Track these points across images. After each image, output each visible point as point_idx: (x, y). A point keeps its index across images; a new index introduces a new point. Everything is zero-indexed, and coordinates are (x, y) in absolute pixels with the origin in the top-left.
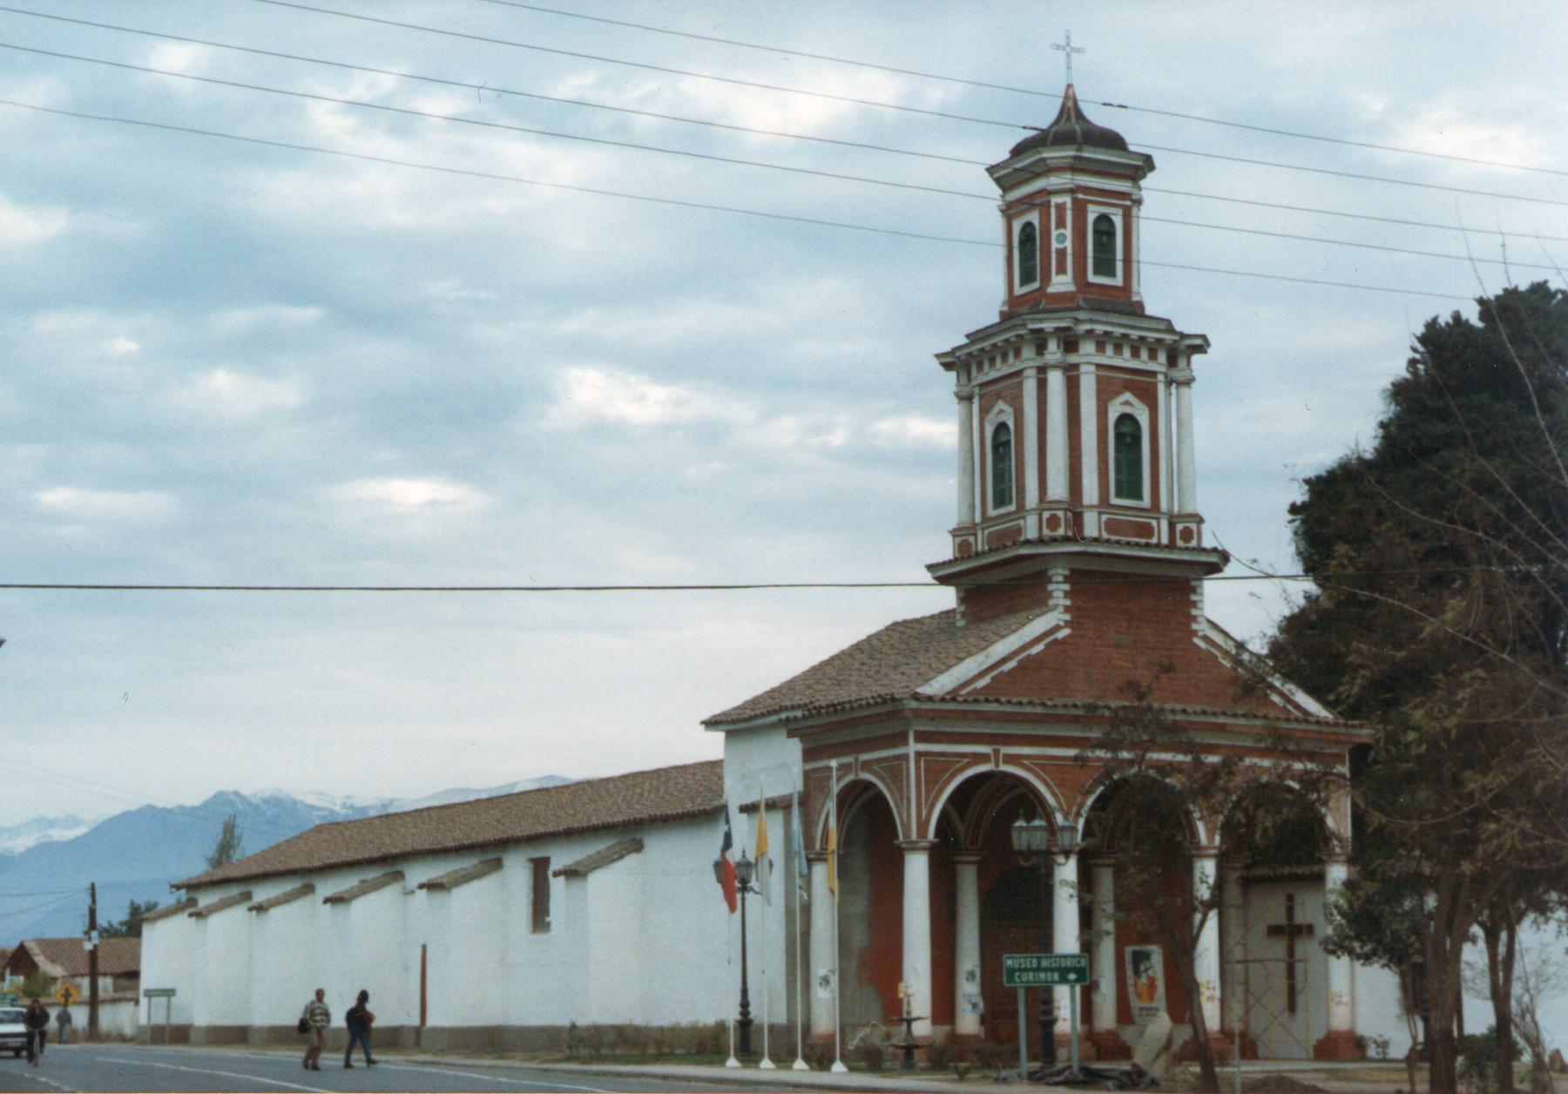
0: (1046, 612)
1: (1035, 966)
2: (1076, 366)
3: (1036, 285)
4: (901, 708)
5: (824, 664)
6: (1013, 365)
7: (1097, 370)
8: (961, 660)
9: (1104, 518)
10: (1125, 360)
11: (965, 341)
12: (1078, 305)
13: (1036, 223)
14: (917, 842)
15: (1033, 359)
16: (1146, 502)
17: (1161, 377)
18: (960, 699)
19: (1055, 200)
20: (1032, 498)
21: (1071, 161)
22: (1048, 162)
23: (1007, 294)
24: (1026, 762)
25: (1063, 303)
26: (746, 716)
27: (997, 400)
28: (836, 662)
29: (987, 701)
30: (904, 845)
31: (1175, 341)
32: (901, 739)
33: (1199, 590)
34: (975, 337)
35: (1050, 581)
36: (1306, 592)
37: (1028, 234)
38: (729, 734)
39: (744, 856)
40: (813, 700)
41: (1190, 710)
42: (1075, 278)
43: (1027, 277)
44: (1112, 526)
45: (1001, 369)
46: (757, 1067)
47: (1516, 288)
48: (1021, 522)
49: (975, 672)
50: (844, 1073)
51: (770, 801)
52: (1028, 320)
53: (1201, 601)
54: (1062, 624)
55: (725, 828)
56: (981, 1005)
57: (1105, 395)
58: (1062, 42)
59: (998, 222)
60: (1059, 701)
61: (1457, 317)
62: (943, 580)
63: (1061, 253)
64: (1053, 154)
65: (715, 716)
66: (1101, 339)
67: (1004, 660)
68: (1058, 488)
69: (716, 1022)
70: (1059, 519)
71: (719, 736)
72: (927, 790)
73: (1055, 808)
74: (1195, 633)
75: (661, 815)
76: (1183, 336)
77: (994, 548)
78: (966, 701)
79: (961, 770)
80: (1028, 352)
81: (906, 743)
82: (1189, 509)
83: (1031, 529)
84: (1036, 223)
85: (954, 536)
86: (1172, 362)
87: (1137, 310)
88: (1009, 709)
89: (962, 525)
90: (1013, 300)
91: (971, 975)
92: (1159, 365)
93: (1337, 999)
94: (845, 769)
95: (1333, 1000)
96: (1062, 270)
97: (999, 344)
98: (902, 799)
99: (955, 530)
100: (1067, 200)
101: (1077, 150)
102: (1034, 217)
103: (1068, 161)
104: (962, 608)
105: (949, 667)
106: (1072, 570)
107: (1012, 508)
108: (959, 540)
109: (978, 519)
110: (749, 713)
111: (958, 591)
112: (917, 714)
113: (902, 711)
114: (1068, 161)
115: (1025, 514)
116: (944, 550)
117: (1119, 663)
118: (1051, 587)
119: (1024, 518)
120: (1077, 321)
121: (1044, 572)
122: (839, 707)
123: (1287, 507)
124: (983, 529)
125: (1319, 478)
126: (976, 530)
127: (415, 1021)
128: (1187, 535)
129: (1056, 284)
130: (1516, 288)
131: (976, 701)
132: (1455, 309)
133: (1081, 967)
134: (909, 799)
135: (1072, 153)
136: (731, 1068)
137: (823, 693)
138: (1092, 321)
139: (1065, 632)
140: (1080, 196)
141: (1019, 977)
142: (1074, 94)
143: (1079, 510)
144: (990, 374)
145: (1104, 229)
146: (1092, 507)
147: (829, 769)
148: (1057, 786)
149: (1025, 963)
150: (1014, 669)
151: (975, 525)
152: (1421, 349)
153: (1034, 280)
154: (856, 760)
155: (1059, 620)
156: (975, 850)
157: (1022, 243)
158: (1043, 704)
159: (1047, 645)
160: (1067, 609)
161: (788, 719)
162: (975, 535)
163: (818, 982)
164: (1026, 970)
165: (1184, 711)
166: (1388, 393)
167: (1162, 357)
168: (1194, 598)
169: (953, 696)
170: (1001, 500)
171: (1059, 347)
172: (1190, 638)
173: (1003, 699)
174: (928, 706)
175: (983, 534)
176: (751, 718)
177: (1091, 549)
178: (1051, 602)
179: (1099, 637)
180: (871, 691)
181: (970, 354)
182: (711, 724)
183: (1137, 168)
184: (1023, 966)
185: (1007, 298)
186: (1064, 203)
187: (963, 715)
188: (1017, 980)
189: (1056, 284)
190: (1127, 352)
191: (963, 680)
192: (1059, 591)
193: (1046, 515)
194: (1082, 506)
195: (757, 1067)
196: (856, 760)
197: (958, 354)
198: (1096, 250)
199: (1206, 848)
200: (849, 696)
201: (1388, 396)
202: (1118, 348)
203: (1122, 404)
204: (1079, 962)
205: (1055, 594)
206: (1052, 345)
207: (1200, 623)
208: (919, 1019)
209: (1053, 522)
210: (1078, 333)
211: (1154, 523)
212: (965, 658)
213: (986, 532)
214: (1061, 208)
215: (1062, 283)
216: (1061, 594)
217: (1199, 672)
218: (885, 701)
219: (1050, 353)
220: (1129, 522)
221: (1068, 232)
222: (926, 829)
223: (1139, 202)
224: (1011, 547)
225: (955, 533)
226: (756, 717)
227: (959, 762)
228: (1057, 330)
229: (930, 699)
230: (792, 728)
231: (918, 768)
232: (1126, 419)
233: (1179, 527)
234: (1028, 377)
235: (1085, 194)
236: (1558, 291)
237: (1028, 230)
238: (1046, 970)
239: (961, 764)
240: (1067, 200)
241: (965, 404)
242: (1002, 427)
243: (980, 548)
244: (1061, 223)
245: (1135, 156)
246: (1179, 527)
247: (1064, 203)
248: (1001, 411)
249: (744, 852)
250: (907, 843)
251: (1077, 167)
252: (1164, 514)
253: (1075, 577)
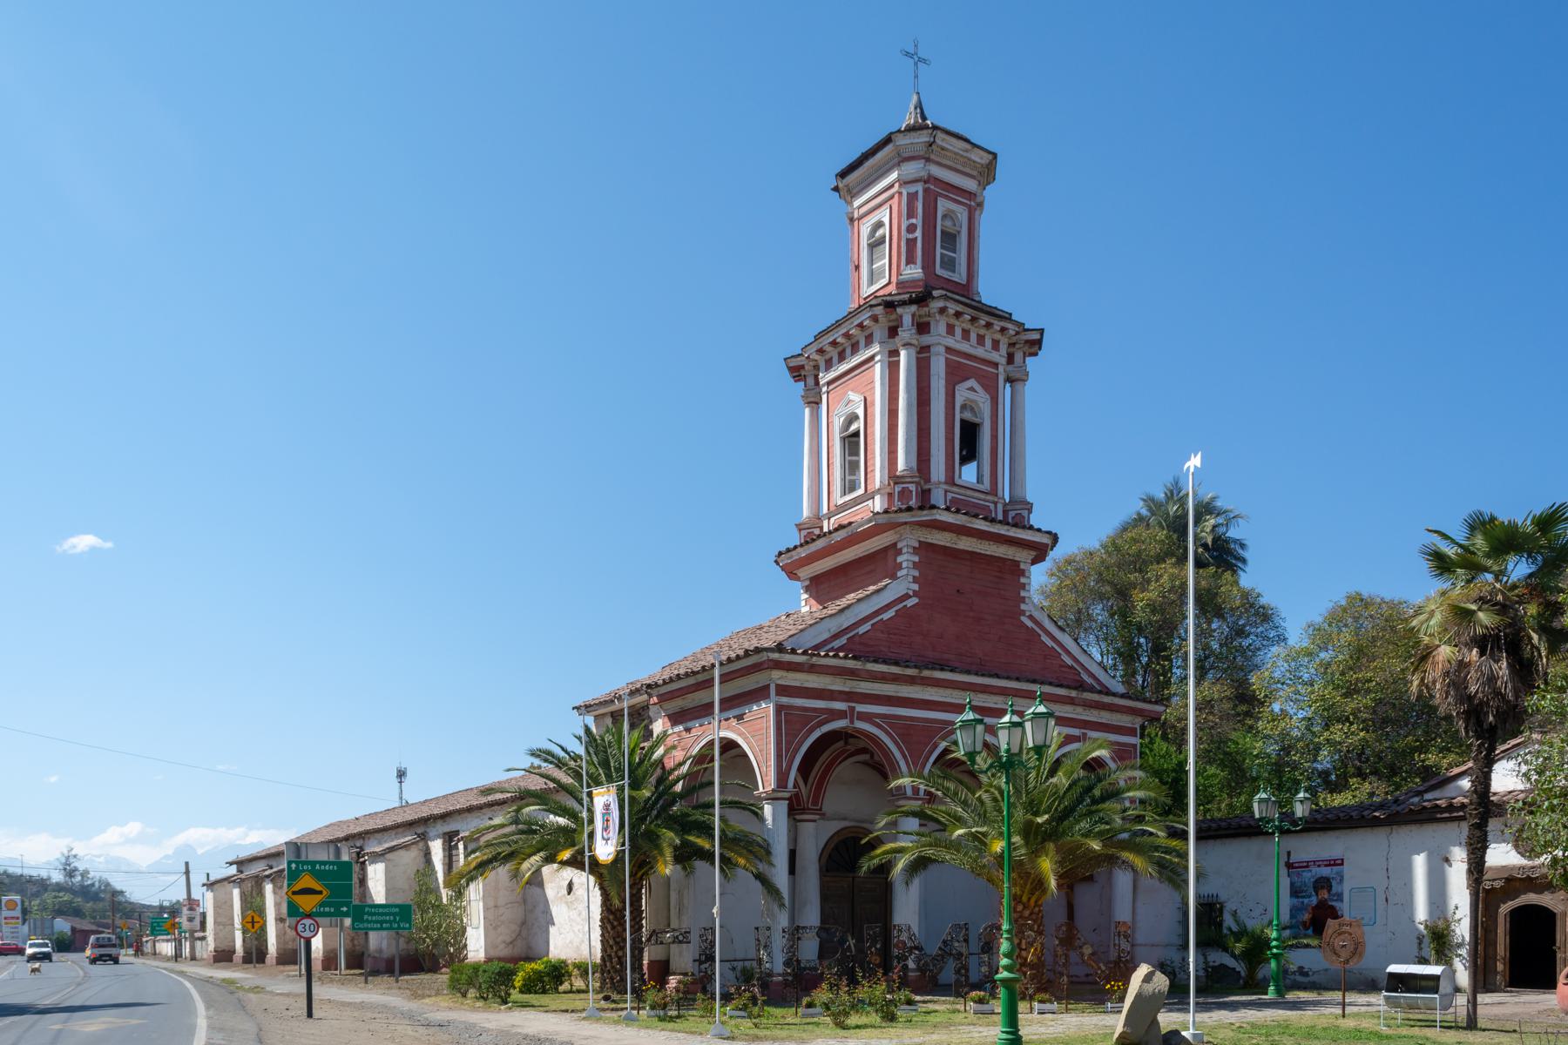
7: (946, 352)
9: (950, 496)
24: (877, 720)
53: (1029, 584)
54: (911, 594)
57: (956, 374)
73: (807, 660)
74: (1023, 613)
96: (607, 807)
127: (1347, 993)
139: (914, 601)
147: (590, 857)
160: (915, 580)
203: (968, 389)
209: (904, 494)
211: (992, 506)
223: (980, 205)
247: (917, 192)
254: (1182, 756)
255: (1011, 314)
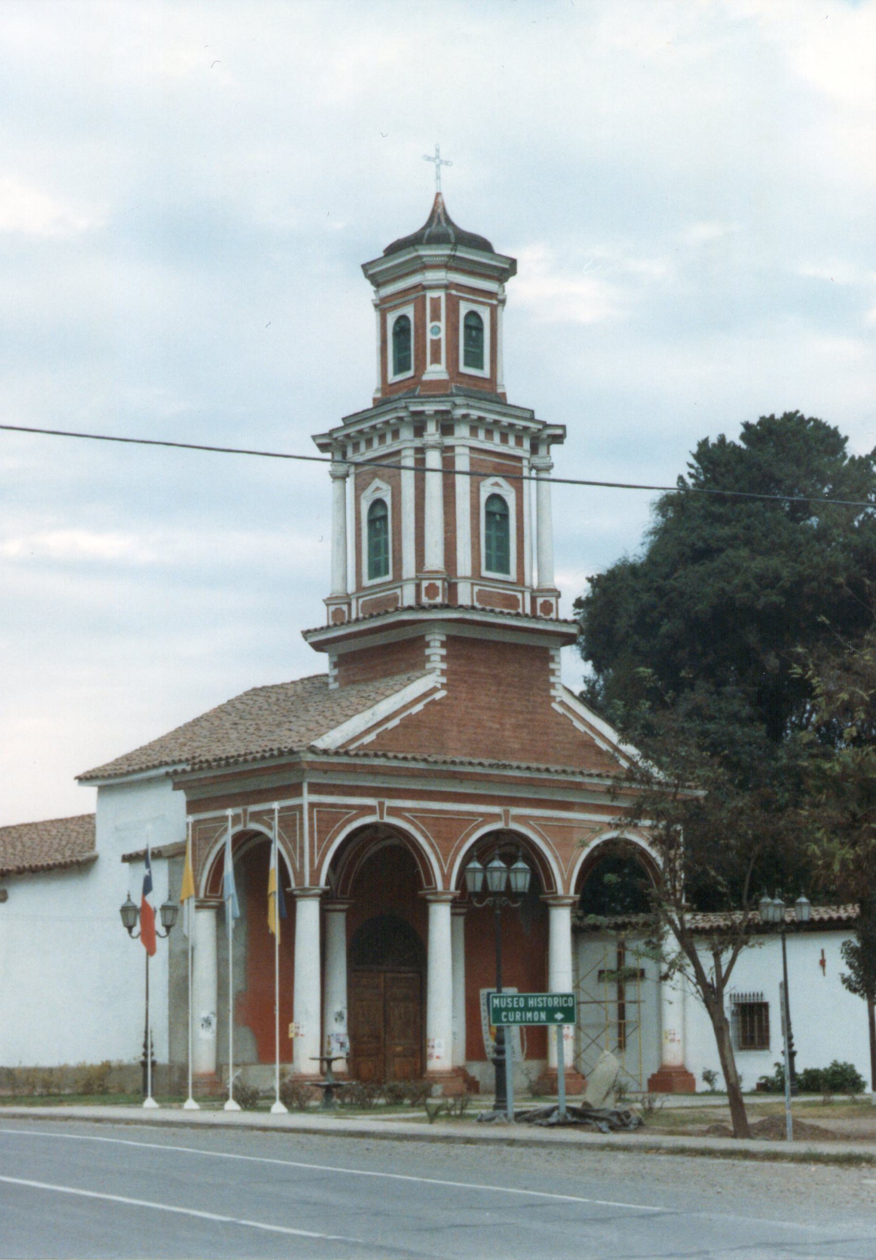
0: (425, 675)
1: (522, 1005)
2: (451, 448)
3: (411, 373)
4: (298, 760)
5: (196, 722)
6: (391, 446)
7: (470, 452)
8: (349, 717)
9: (476, 588)
10: (495, 444)
11: (341, 424)
12: (452, 393)
13: (411, 316)
14: (309, 889)
15: (412, 441)
16: (513, 576)
17: (525, 462)
18: (352, 753)
19: (430, 295)
20: (409, 568)
21: (446, 259)
22: (424, 259)
23: (380, 382)
24: (407, 814)
25: (437, 389)
26: (124, 771)
27: (373, 478)
28: (204, 724)
29: (376, 755)
30: (296, 892)
31: (539, 430)
32: (295, 790)
33: (557, 659)
34: (349, 421)
35: (427, 645)
36: (585, 677)
37: (402, 328)
38: (102, 790)
39: (129, 900)
40: (196, 755)
41: (552, 769)
42: (447, 367)
43: (401, 365)
44: (481, 596)
45: (378, 450)
46: (181, 1107)
47: (772, 417)
48: (398, 591)
49: (363, 728)
50: (155, 1109)
51: (156, 851)
52: (411, 402)
53: (559, 670)
54: (439, 686)
55: (146, 872)
56: (348, 1045)
57: (477, 475)
58: (433, 154)
59: (372, 318)
60: (441, 758)
61: (722, 439)
62: (318, 646)
63: (436, 344)
64: (425, 252)
65: (88, 772)
66: (475, 424)
67: (388, 719)
68: (435, 559)
69: (835, 1064)
70: (438, 588)
71: (91, 791)
72: (319, 838)
75: (30, 866)
76: (546, 426)
77: (375, 613)
78: (357, 755)
79: (349, 821)
80: (406, 434)
81: (300, 794)
82: (547, 585)
83: (408, 596)
84: (411, 316)
85: (328, 605)
86: (534, 450)
87: (500, 399)
88: (395, 763)
89: (334, 596)
90: (386, 387)
91: (340, 1015)
92: (523, 451)
93: (670, 1037)
94: (236, 819)
95: (667, 1038)
96: (436, 360)
97: (352, 435)
98: (295, 848)
99: (329, 599)
100: (441, 294)
101: (452, 250)
102: (409, 311)
103: (443, 259)
104: (335, 672)
105: (339, 723)
106: (448, 636)
107: (389, 577)
108: (332, 608)
109: (351, 588)
110: (125, 768)
111: (331, 656)
112: (312, 766)
113: (298, 763)
114: (443, 259)
115: (402, 583)
116: (320, 618)
117: (489, 724)
118: (428, 652)
119: (401, 587)
120: (455, 405)
121: (422, 637)
122: (231, 760)
123: (573, 601)
124: (358, 598)
125: (600, 576)
126: (351, 599)
128: (547, 607)
129: (430, 373)
130: (772, 417)
131: (366, 755)
132: (721, 432)
133: (568, 1007)
134: (302, 848)
135: (448, 252)
136: (148, 1109)
137: (204, 749)
138: (468, 406)
139: (438, 696)
140: (454, 292)
141: (506, 1017)
142: (443, 200)
143: (454, 581)
144: (367, 454)
145: (474, 325)
146: (465, 578)
148: (434, 837)
149: (512, 1002)
150: (397, 727)
151: (348, 595)
152: (696, 465)
153: (408, 368)
154: (245, 811)
155: (436, 682)
156: (344, 899)
157: (396, 334)
158: (425, 760)
159: (426, 705)
160: (443, 673)
161: (175, 772)
162: (349, 605)
163: (200, 1026)
164: (513, 1009)
165: (547, 770)
166: (655, 505)
167: (527, 444)
168: (552, 666)
169: (342, 751)
170: (376, 569)
171: (437, 430)
172: (549, 703)
173: (391, 754)
174: (324, 759)
175: (357, 602)
176: (128, 773)
177: (468, 616)
178: (428, 666)
179: (471, 700)
180: (260, 746)
181: (348, 436)
182: (84, 779)
183: (504, 270)
184: (510, 1006)
185: (380, 386)
186: (439, 298)
187: (352, 769)
188: (504, 1020)
189: (430, 373)
190: (497, 438)
191: (351, 735)
192: (436, 651)
193: (425, 584)
194: (456, 577)
195: (181, 1107)
196: (245, 811)
197: (335, 435)
198: (466, 344)
199: (563, 898)
200: (236, 751)
201: (656, 509)
202: (489, 433)
204: (566, 1002)
205: (432, 658)
206: (431, 427)
207: (558, 690)
208: (336, 1059)
210: (455, 417)
211: (519, 596)
212: (352, 716)
213: (361, 601)
214: (436, 302)
215: (436, 372)
216: (438, 658)
217: (557, 735)
218: (281, 753)
219: (429, 435)
220: (499, 593)
221: (442, 324)
222: (318, 878)
223: (503, 302)
224: (393, 612)
225: (328, 602)
226: (134, 772)
227: (348, 813)
228: (437, 412)
229: (325, 752)
230: (178, 781)
231: (311, 819)
232: (496, 498)
233: (540, 601)
234: (406, 457)
235: (457, 290)
236: (811, 419)
237: (403, 323)
238: (533, 1010)
239: (351, 814)
240: (441, 294)
241: (338, 483)
242: (378, 503)
243: (354, 616)
244: (436, 317)
245: (503, 260)
246: (540, 601)
247: (439, 298)
248: (378, 489)
249: (129, 896)
250: (300, 890)
251: (453, 264)
252: (527, 587)
253: (451, 642)
254: (718, 1155)
255: (533, 412)
